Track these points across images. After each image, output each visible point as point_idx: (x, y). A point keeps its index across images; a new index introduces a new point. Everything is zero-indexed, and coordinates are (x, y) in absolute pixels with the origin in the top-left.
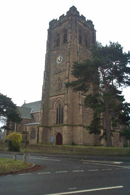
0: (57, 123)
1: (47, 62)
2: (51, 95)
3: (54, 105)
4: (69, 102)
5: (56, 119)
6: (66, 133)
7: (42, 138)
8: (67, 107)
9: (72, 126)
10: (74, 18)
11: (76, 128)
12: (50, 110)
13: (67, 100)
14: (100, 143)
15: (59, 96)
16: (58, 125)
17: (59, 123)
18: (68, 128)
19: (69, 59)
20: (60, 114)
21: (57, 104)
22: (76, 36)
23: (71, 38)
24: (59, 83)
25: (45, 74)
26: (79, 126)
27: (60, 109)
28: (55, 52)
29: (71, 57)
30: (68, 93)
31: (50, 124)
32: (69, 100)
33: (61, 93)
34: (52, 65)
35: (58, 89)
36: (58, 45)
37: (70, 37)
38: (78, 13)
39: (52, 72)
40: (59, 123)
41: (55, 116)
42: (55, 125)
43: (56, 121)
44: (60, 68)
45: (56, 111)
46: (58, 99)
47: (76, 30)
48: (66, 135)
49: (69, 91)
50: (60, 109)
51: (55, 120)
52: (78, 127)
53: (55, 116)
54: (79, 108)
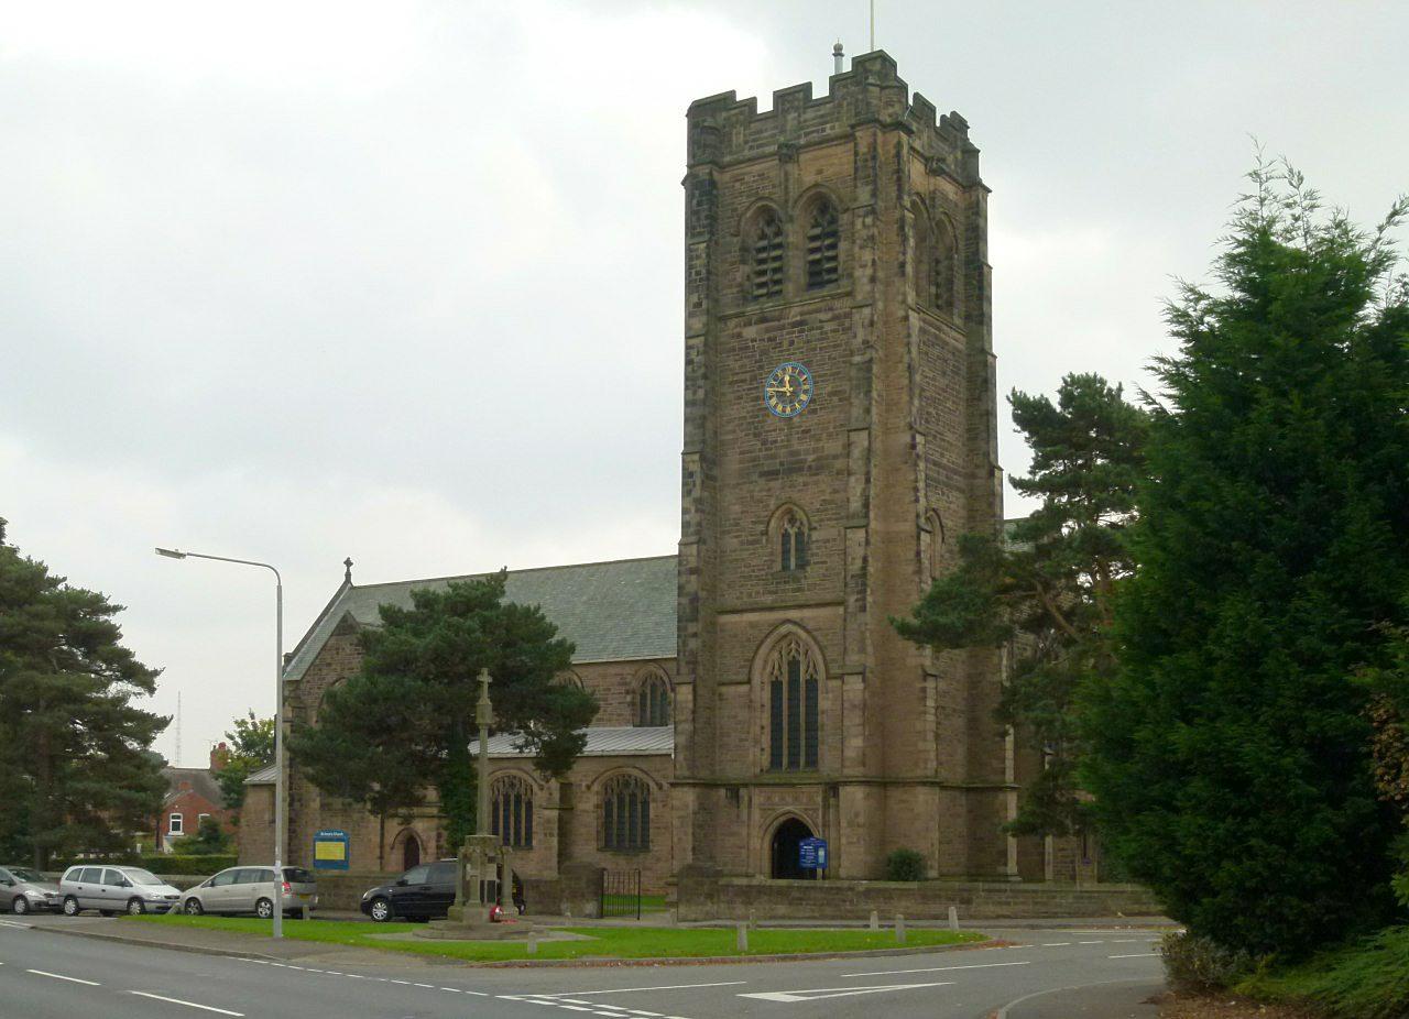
0: (776, 761)
1: (701, 394)
2: (731, 599)
3: (758, 663)
4: (870, 662)
5: (766, 741)
6: (861, 820)
7: (694, 849)
8: (861, 686)
9: (883, 783)
10: (893, 137)
11: (905, 797)
12: (724, 689)
13: (862, 650)
14: (1001, 869)
15: (794, 614)
16: (774, 777)
17: (794, 763)
18: (868, 796)
19: (868, 411)
20: (794, 715)
21: (776, 655)
22: (902, 265)
23: (873, 279)
24: (786, 536)
25: (695, 467)
26: (924, 784)
27: (794, 681)
28: (750, 332)
29: (874, 394)
30: (863, 609)
31: (733, 771)
32: (870, 649)
33: (801, 598)
34: (736, 411)
35: (778, 567)
36: (770, 283)
37: (869, 271)
38: (903, 87)
39: (732, 463)
40: (794, 763)
41: (763, 728)
42: (766, 778)
43: (768, 751)
44: (796, 446)
45: (766, 695)
46: (784, 629)
47: (902, 223)
48: (861, 830)
49: (869, 599)
50: (794, 681)
51: (763, 750)
52: (921, 790)
53: (763, 728)
54: (924, 690)
